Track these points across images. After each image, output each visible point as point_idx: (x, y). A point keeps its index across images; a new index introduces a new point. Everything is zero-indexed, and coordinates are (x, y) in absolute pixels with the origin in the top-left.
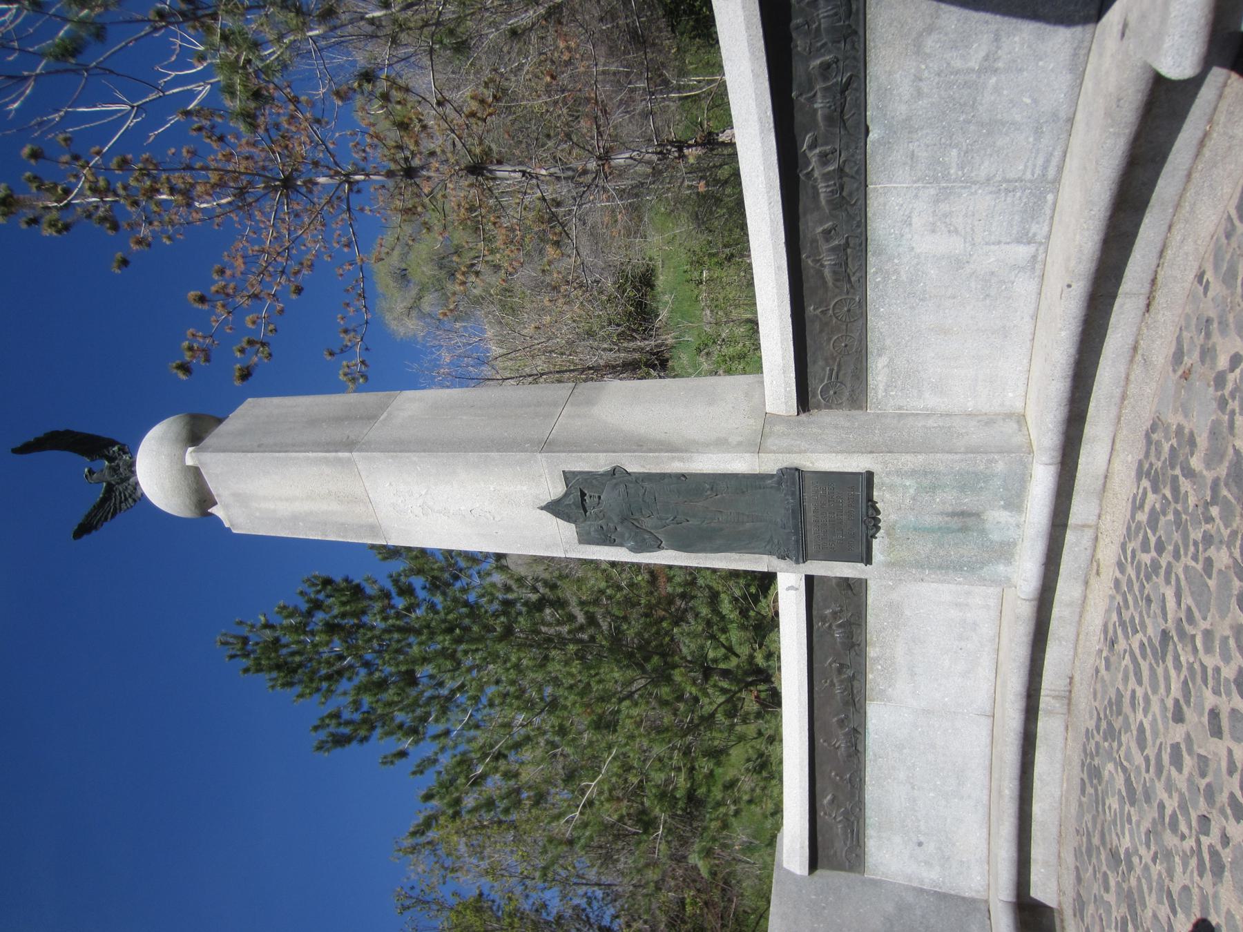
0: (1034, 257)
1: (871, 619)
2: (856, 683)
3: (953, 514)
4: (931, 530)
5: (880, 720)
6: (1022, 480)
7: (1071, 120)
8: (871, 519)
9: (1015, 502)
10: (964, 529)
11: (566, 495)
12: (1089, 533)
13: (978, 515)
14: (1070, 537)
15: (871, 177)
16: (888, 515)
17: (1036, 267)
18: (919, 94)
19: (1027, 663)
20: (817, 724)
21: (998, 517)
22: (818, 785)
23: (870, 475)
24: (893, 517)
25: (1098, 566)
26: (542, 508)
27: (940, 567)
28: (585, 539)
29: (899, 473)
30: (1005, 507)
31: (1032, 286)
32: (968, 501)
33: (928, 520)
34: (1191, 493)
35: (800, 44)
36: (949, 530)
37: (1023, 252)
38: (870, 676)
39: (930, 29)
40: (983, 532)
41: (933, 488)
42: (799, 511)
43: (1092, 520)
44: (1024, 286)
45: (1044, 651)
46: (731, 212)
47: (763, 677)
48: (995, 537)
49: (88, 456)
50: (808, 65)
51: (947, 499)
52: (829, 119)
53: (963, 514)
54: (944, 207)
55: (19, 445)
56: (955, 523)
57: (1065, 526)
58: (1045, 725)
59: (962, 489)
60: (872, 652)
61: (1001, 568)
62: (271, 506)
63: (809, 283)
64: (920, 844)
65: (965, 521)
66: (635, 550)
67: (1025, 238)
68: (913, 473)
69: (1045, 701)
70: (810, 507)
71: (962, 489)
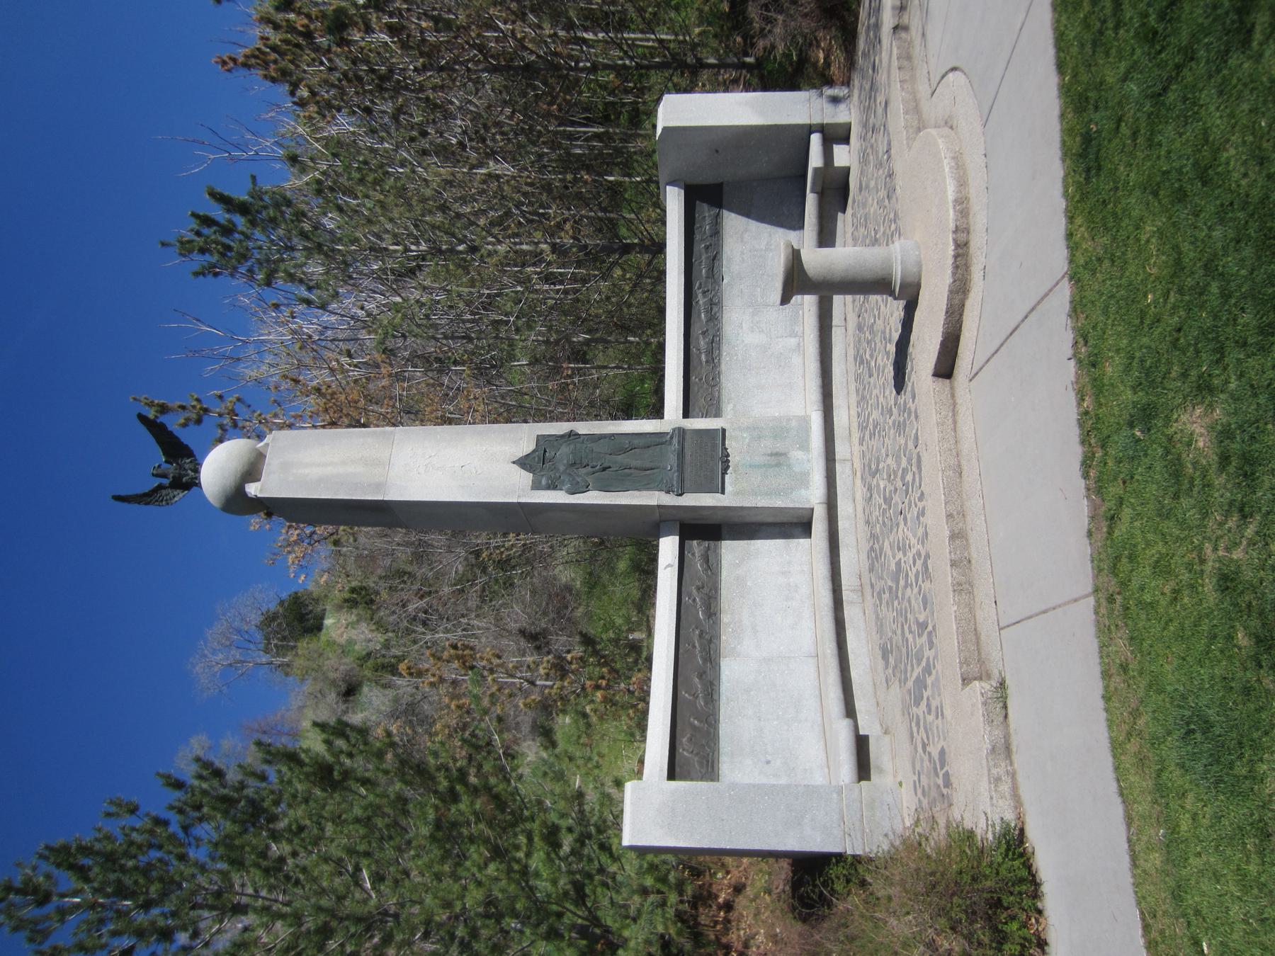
1: (724, 592)
2: (712, 646)
3: (771, 455)
4: (759, 467)
5: (732, 672)
9: (805, 446)
10: (778, 465)
11: (534, 451)
12: (849, 464)
13: (785, 454)
14: (838, 467)
16: (733, 459)
17: (799, 348)
19: (854, 752)
20: (680, 679)
21: (796, 455)
22: (679, 728)
23: (724, 431)
25: (914, 768)
27: (767, 494)
28: (536, 486)
30: (799, 449)
31: (800, 360)
32: (780, 447)
35: (697, 237)
36: (771, 466)
38: (723, 638)
39: (746, 230)
40: (789, 466)
42: (681, 454)
43: (848, 456)
45: (838, 556)
46: (654, 354)
47: (640, 656)
48: (796, 469)
49: (165, 453)
50: (699, 247)
51: (768, 445)
52: (707, 277)
53: (777, 454)
54: (756, 318)
56: (773, 460)
57: (834, 460)
58: (849, 613)
59: (775, 437)
61: (803, 492)
62: (307, 471)
63: (694, 363)
64: (768, 762)
65: (778, 459)
66: (572, 492)
67: (793, 334)
69: (846, 595)
70: (688, 452)
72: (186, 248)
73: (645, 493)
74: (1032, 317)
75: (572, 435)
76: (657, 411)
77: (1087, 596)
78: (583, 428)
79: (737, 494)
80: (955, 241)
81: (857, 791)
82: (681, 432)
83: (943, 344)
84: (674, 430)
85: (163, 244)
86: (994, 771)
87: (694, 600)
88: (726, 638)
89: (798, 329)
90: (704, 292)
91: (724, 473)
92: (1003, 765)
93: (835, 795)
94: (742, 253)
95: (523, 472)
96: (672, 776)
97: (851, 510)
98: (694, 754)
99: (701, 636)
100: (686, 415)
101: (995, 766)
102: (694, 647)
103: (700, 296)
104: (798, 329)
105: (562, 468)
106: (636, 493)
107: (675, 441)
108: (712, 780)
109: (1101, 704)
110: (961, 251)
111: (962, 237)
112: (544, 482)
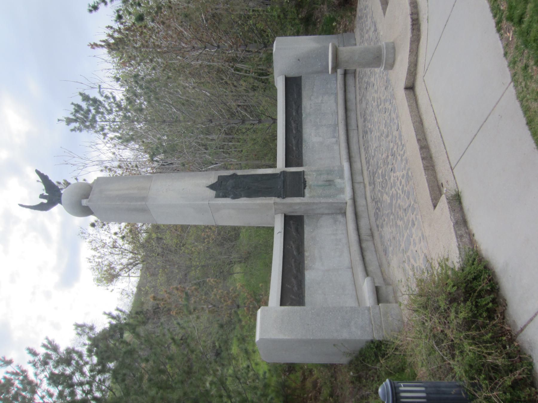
0: (337, 141)
3: (327, 181)
4: (321, 186)
5: (310, 276)
6: (342, 170)
7: (337, 112)
8: (304, 184)
9: (342, 177)
10: (330, 185)
11: (216, 182)
15: (303, 125)
17: (338, 143)
18: (311, 108)
21: (338, 181)
24: (311, 183)
26: (207, 187)
27: (325, 197)
29: (311, 171)
32: (330, 177)
33: (320, 183)
34: (387, 198)
36: (326, 186)
37: (334, 140)
38: (306, 262)
39: (312, 95)
40: (335, 186)
41: (321, 174)
42: (284, 182)
44: (336, 147)
48: (338, 186)
51: (325, 177)
53: (329, 181)
55: (42, 172)
59: (328, 174)
60: (306, 254)
61: (342, 196)
65: (330, 183)
68: (315, 171)
71: (328, 174)
72: (69, 121)
73: (267, 198)
74: (439, 135)
75: (234, 176)
76: (274, 166)
77: (511, 83)
78: (240, 173)
79: (310, 197)
80: (412, 18)
81: (378, 308)
82: (284, 173)
83: (409, 69)
84: (281, 172)
85: (59, 120)
86: (459, 232)
87: (292, 247)
88: (307, 262)
89: (336, 135)
90: (294, 122)
91: (304, 189)
92: (463, 229)
93: (366, 311)
94: (311, 105)
95: (212, 191)
96: (282, 304)
97: (364, 203)
98: (293, 294)
99: (295, 262)
100: (287, 166)
101: (459, 230)
102: (292, 266)
103: (292, 123)
104: (336, 135)
105: (229, 189)
106: (264, 198)
107: (282, 177)
108: (303, 306)
109: (526, 128)
110: (415, 23)
111: (415, 17)
112: (221, 194)
